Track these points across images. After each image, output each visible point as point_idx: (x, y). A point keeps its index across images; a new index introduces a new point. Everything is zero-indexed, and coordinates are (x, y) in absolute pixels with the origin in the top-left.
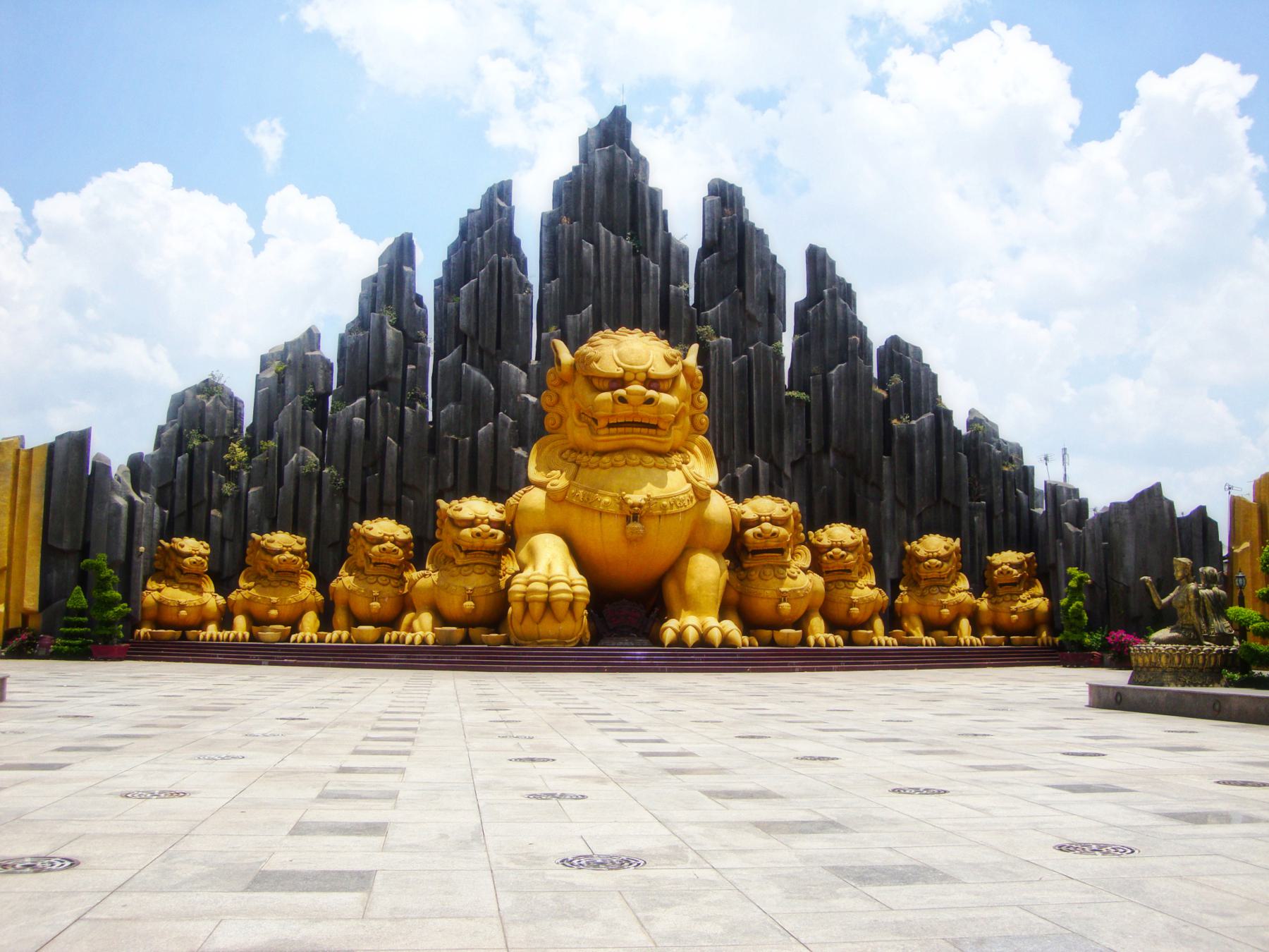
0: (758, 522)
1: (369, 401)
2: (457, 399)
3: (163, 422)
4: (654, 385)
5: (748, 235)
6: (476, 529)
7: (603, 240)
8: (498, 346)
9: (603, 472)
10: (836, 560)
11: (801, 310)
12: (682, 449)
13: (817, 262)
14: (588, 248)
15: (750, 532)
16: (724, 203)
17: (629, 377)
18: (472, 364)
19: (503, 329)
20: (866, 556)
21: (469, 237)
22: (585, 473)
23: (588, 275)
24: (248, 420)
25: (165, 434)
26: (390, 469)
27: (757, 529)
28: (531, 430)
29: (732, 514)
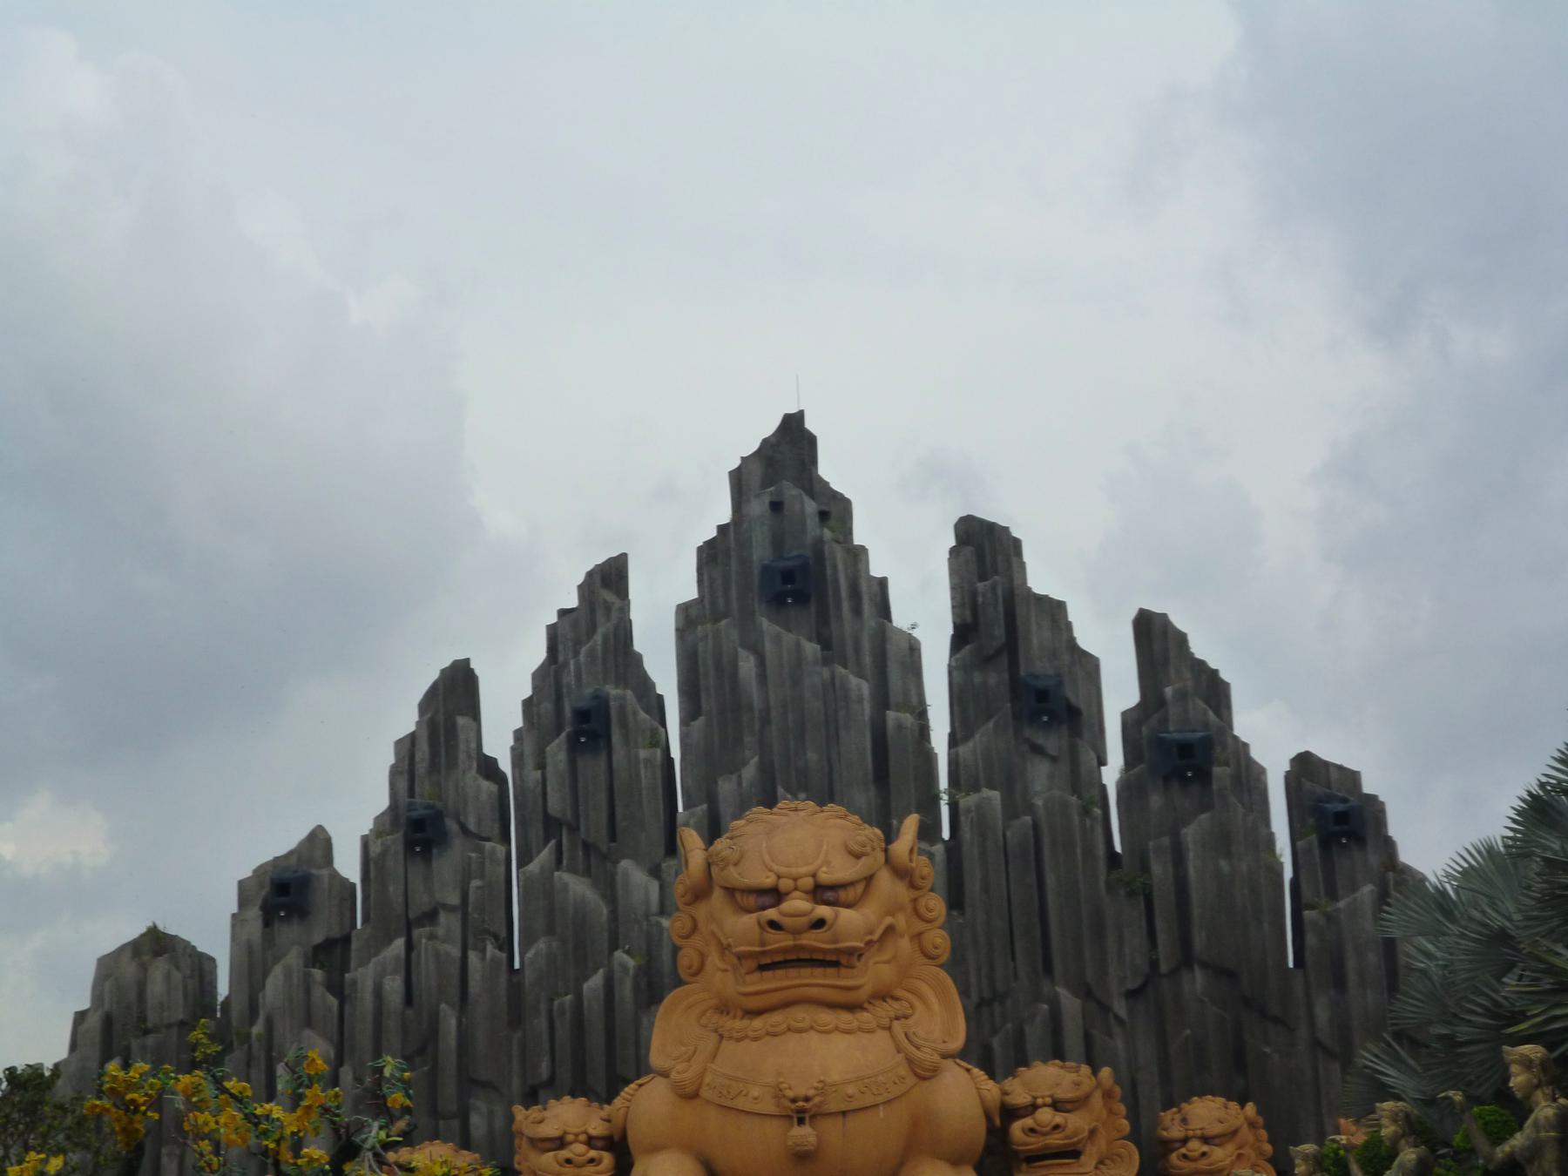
0: (1033, 1108)
1: (410, 946)
2: (550, 930)
3: (84, 1003)
4: (829, 895)
5: (1020, 610)
6: (564, 1154)
7: (769, 647)
8: (613, 836)
9: (754, 1045)
10: (1195, 1160)
11: (1131, 722)
12: (899, 993)
13: (1155, 638)
14: (747, 666)
15: (1017, 1128)
16: (983, 553)
17: (785, 884)
18: (573, 870)
19: (619, 810)
20: (1261, 1154)
21: (561, 659)
22: (728, 1046)
23: (750, 708)
24: (223, 989)
25: (85, 1026)
26: (449, 1061)
27: (1028, 1122)
28: (655, 985)
29: (982, 1100)
